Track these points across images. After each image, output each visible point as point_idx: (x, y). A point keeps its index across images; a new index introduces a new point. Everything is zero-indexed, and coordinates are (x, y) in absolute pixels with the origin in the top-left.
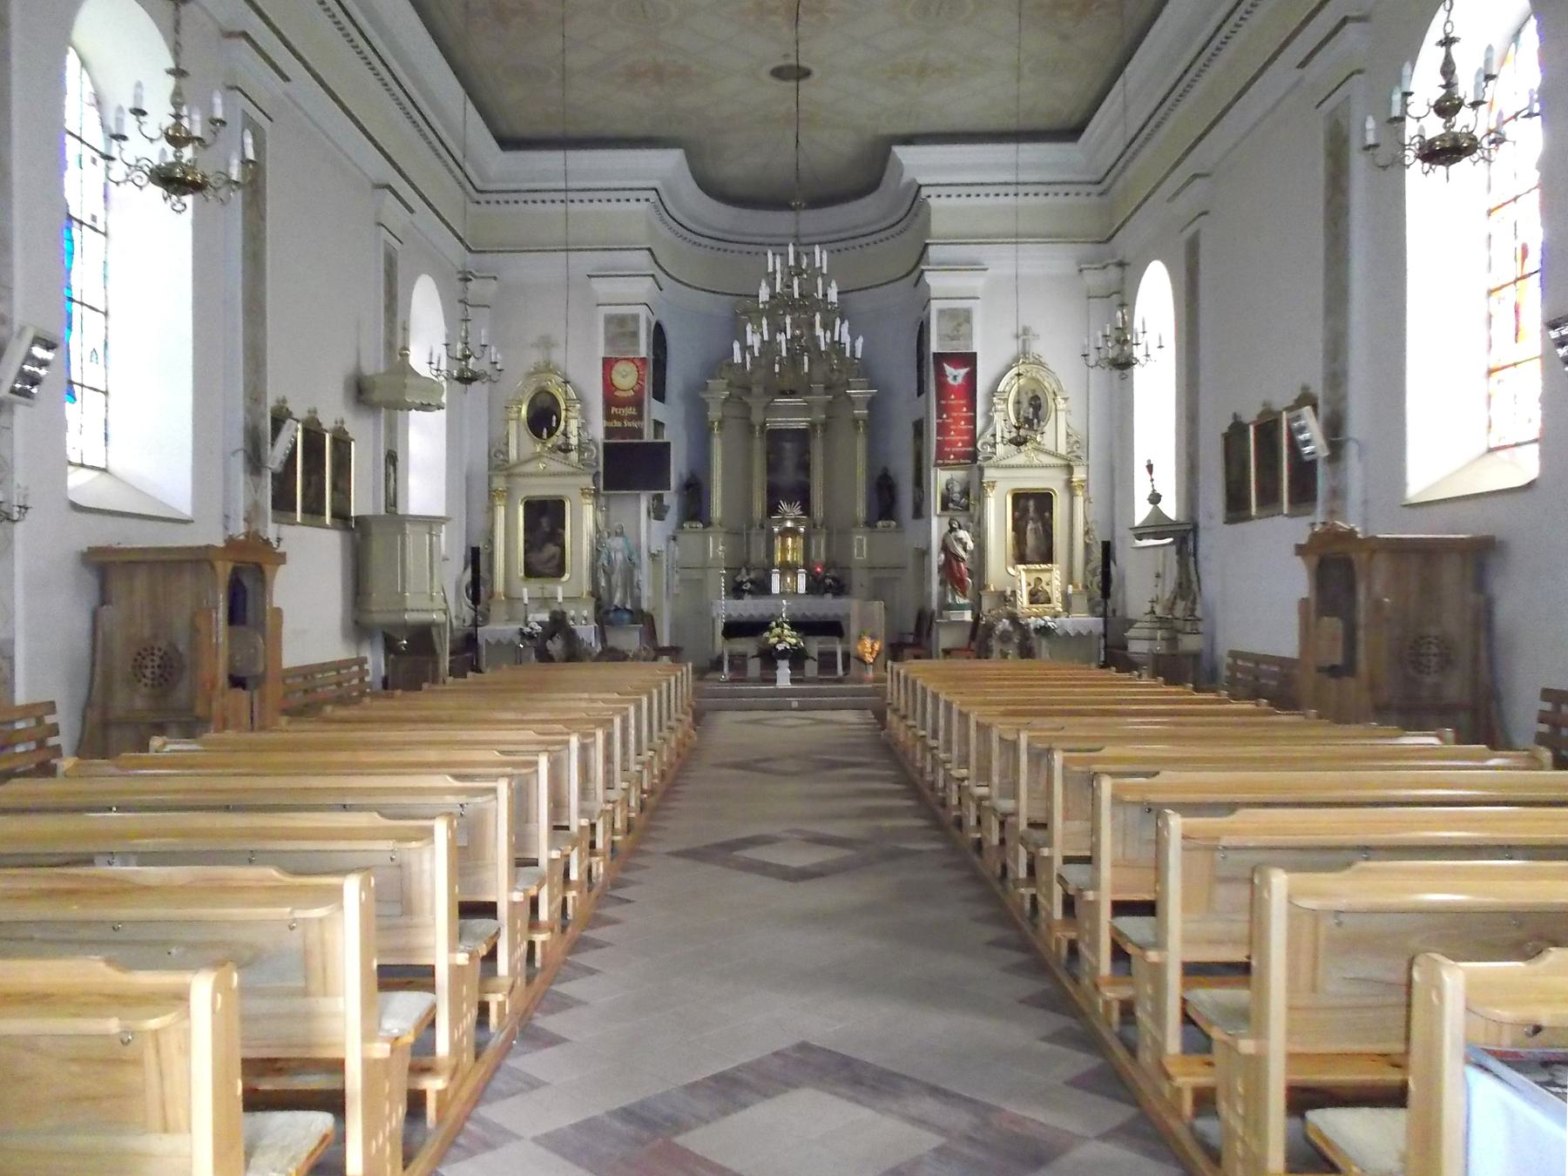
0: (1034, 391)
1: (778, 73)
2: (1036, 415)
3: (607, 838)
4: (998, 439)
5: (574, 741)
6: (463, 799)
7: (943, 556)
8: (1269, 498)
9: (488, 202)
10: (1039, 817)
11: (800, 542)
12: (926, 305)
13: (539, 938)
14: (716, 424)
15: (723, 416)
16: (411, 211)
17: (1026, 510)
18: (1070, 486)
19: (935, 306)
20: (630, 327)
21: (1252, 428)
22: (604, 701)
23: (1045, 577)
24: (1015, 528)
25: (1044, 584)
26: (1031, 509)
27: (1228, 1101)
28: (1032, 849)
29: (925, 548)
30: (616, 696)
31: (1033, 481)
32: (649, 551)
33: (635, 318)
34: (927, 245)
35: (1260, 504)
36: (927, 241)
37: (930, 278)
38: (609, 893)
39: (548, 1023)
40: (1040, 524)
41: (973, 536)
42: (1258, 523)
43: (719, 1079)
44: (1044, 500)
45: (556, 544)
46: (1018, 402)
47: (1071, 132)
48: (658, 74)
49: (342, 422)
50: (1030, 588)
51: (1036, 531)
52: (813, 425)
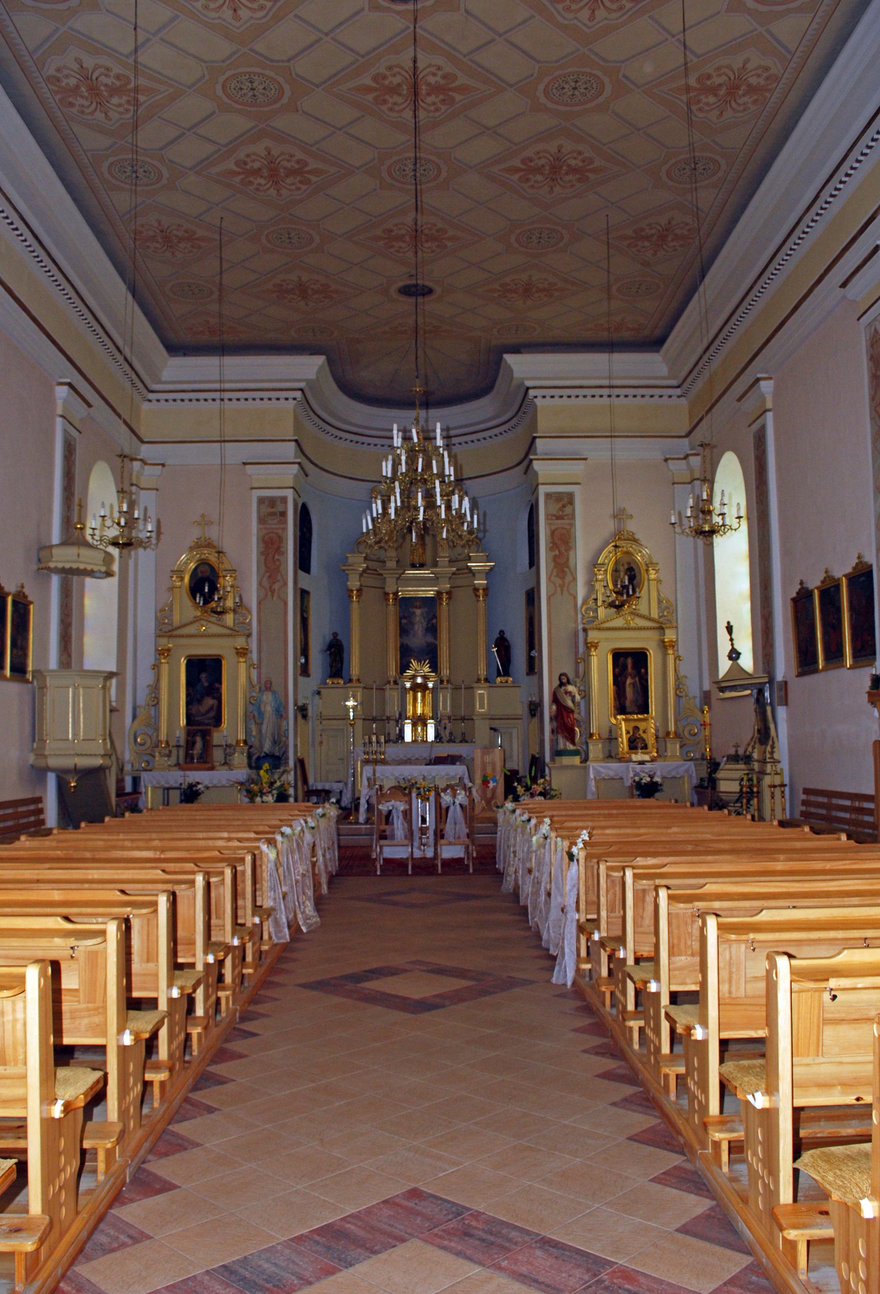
0: (629, 563)
1: (407, 291)
2: (632, 579)
3: (236, 971)
4: (600, 603)
5: (200, 879)
6: (72, 942)
7: (554, 707)
8: (834, 654)
9: (158, 401)
10: (646, 950)
11: (429, 697)
12: (535, 490)
13: (156, 1077)
14: (355, 592)
15: (361, 585)
16: (89, 405)
17: (625, 667)
18: (664, 646)
19: (542, 490)
20: (280, 508)
21: (816, 593)
22: (240, 840)
23: (642, 726)
24: (615, 682)
25: (641, 732)
26: (630, 666)
27: (847, 1261)
28: (640, 985)
29: (538, 701)
30: (253, 835)
31: (629, 642)
32: (295, 704)
33: (284, 500)
34: (535, 438)
35: (827, 659)
36: (535, 435)
37: (536, 465)
38: (237, 1026)
39: (161, 1168)
40: (637, 679)
41: (580, 691)
42: (823, 674)
43: (327, 1231)
44: (640, 658)
45: (214, 698)
46: (616, 571)
47: (655, 343)
48: (303, 290)
49: (23, 587)
50: (629, 735)
51: (634, 685)
52: (439, 593)
